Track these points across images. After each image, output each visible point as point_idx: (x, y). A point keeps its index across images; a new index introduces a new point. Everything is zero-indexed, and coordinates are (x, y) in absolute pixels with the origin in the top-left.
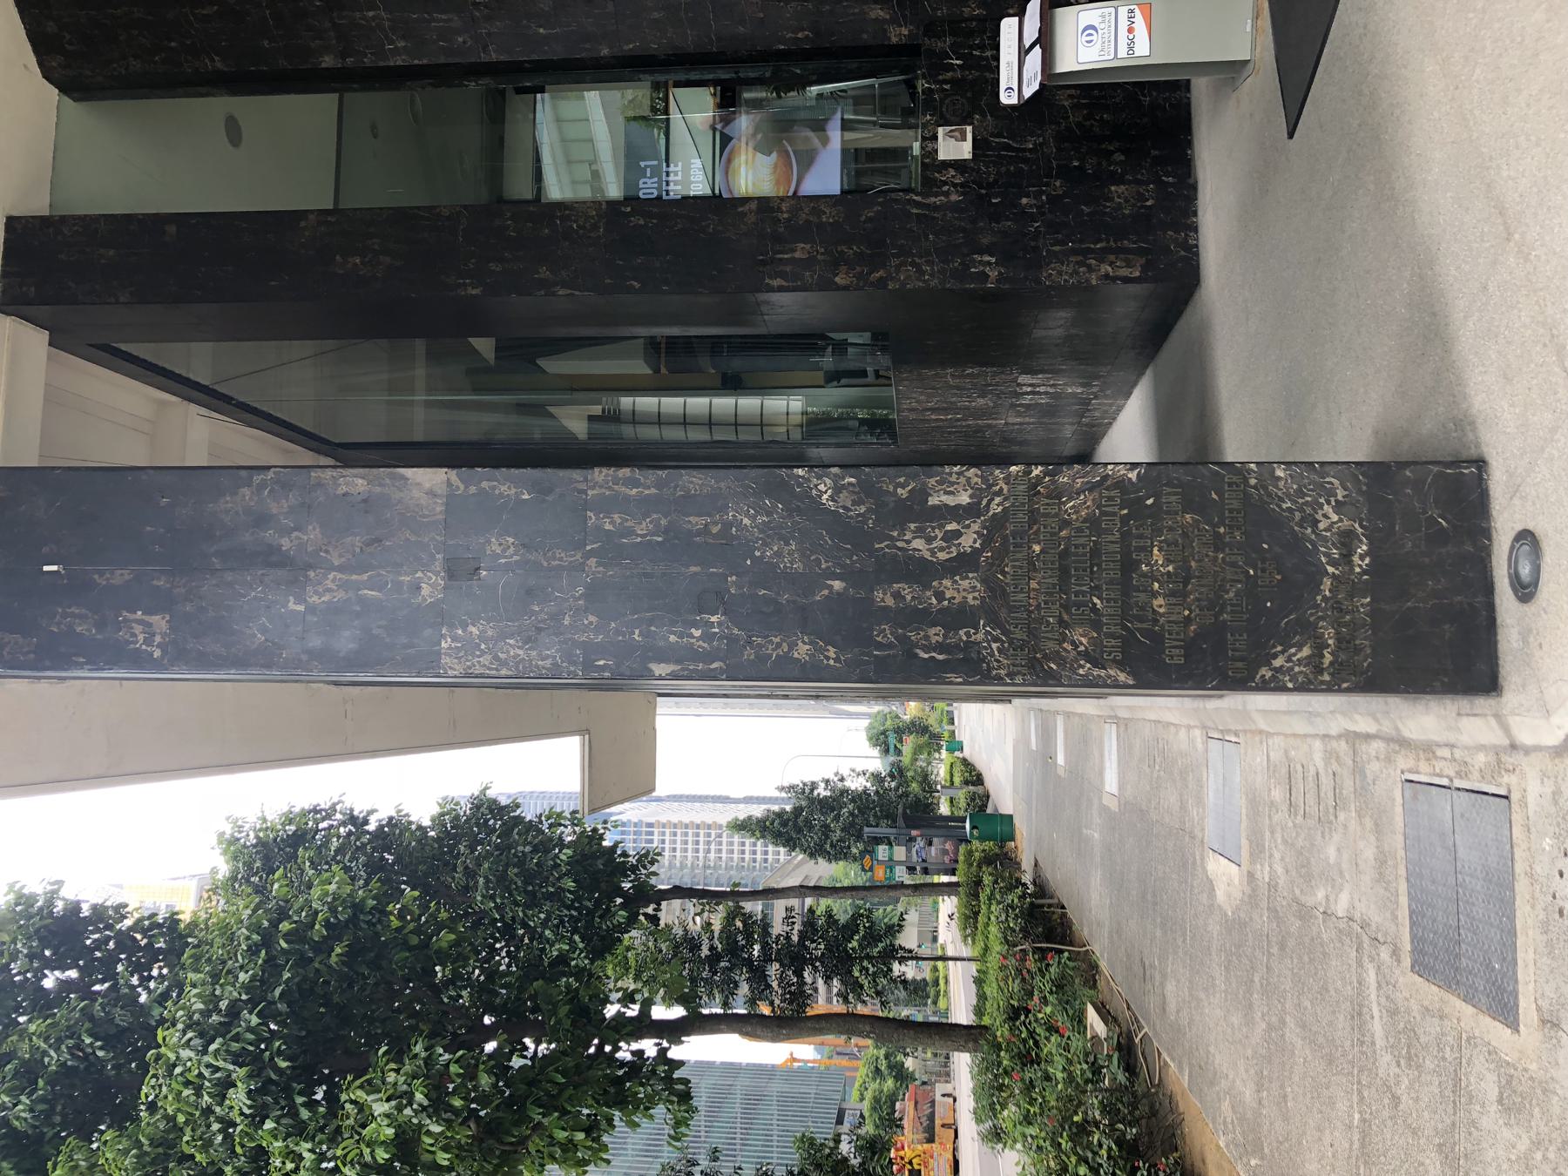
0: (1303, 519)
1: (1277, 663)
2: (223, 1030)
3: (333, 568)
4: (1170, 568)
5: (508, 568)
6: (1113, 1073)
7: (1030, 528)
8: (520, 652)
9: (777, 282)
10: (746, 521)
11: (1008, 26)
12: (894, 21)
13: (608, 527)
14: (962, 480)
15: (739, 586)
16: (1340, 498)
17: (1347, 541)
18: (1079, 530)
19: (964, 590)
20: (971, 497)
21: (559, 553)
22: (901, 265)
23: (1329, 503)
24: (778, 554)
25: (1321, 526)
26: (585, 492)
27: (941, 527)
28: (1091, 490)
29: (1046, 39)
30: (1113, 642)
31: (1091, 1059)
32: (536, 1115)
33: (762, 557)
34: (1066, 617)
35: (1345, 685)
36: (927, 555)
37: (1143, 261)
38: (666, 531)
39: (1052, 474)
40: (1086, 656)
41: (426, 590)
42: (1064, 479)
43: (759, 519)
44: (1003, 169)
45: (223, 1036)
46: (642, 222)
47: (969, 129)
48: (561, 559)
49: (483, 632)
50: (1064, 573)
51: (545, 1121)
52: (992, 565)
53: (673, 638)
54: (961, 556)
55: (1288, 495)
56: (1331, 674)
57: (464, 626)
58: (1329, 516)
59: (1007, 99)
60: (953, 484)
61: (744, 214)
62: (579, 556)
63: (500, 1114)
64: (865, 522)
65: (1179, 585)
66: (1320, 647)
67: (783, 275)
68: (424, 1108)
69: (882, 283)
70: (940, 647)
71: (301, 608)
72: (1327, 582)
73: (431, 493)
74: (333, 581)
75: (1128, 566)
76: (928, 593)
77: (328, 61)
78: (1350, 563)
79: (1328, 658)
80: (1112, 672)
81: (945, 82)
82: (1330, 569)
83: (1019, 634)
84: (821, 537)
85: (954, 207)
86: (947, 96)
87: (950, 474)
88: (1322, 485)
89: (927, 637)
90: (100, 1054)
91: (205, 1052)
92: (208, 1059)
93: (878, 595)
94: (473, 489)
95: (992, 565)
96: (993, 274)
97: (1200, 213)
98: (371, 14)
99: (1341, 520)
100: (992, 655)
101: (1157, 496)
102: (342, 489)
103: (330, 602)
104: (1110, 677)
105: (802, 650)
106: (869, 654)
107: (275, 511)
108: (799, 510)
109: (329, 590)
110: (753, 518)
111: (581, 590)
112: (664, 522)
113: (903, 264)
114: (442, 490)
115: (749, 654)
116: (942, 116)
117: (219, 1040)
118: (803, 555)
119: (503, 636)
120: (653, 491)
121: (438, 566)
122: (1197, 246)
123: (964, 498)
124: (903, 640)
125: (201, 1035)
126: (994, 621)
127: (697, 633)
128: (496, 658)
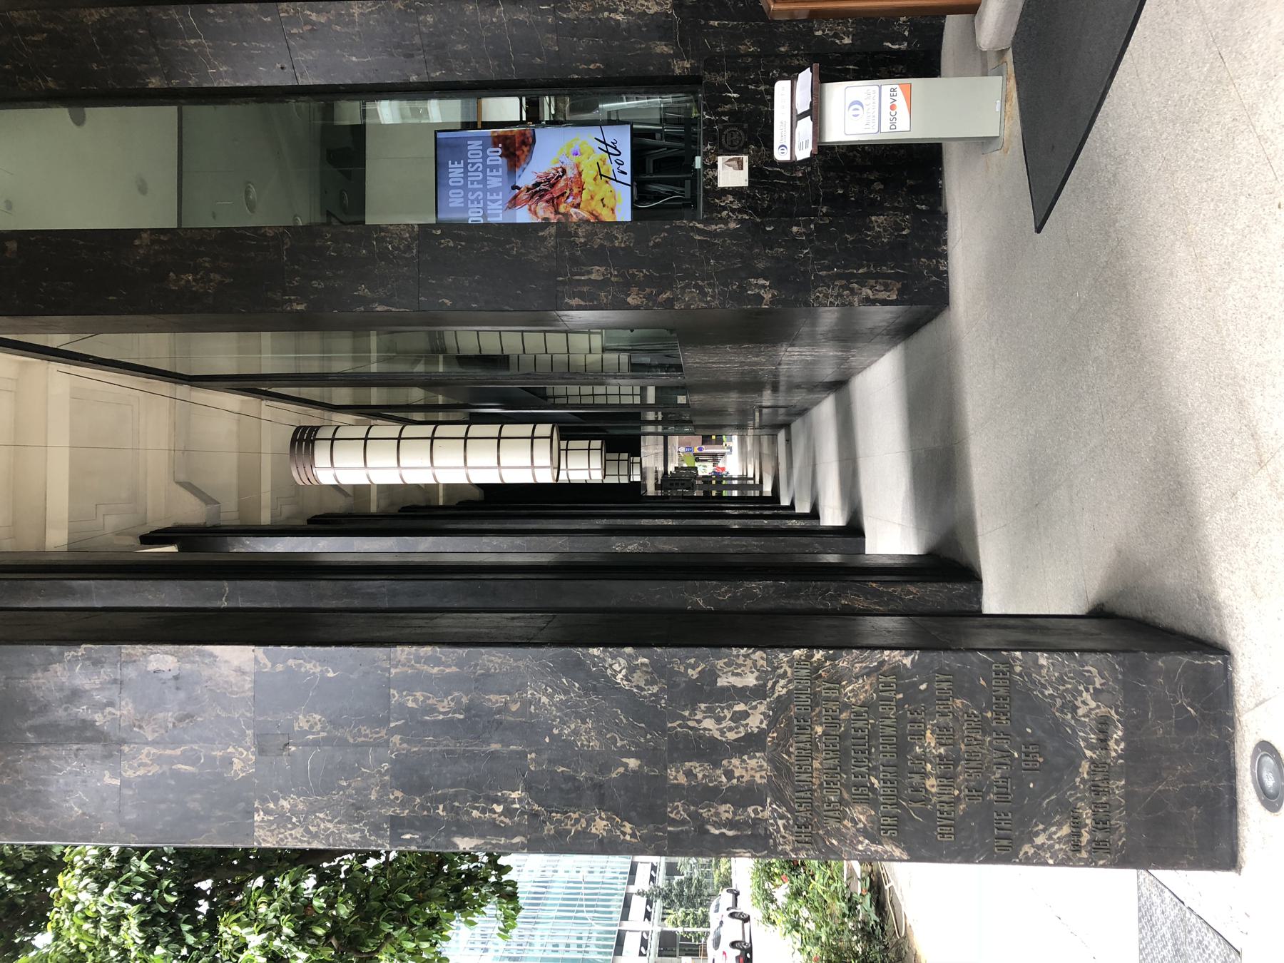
0: (1063, 706)
1: (1039, 840)
2: (115, 875)
3: (147, 743)
4: (942, 750)
5: (316, 743)
6: (866, 907)
7: (813, 710)
8: (330, 825)
9: (574, 302)
10: (544, 700)
11: (782, 89)
12: (677, 56)
13: (410, 704)
14: (749, 662)
15: (538, 764)
16: (1098, 686)
17: (1103, 726)
18: (858, 714)
19: (752, 769)
20: (757, 679)
21: (365, 730)
22: (683, 288)
23: (1087, 690)
24: (576, 732)
25: (1080, 712)
26: (388, 670)
27: (730, 707)
28: (868, 675)
29: (816, 112)
30: (890, 821)
31: (848, 896)
32: (387, 928)
33: (560, 735)
34: (846, 796)
35: (1101, 862)
36: (717, 735)
37: (899, 285)
38: (468, 709)
39: (833, 659)
40: (865, 833)
41: (238, 764)
42: (843, 664)
43: (557, 698)
44: (776, 196)
45: (116, 879)
46: (451, 244)
47: (746, 158)
48: (366, 736)
49: (294, 806)
50: (843, 755)
51: (396, 934)
52: (778, 745)
53: (475, 813)
54: (749, 737)
55: (1050, 683)
56: (1089, 852)
57: (276, 800)
58: (1088, 704)
59: (781, 155)
60: (740, 666)
61: (544, 239)
62: (383, 733)
63: (358, 928)
64: (657, 701)
65: (948, 765)
66: (1077, 826)
67: (581, 295)
68: (291, 939)
69: (669, 303)
70: (730, 824)
71: (117, 782)
72: (1085, 767)
73: (240, 671)
74: (148, 755)
75: (902, 748)
76: (718, 772)
77: (154, 82)
78: (1106, 748)
79: (1086, 837)
80: (888, 848)
81: (724, 114)
82: (1088, 753)
83: (803, 815)
84: (617, 716)
85: (732, 234)
86: (725, 128)
87: (737, 656)
88: (1081, 674)
89: (717, 814)
90: (11, 886)
91: (100, 892)
92: (101, 899)
93: (671, 773)
94: (280, 667)
95: (778, 745)
96: (767, 296)
97: (950, 243)
98: (193, 41)
99: (1098, 707)
100: (778, 831)
101: (930, 682)
102: (152, 667)
103: (145, 776)
104: (886, 852)
105: (600, 826)
106: (664, 831)
107: (87, 687)
108: (595, 689)
109: (145, 765)
110: (551, 697)
111: (386, 766)
112: (465, 700)
113: (688, 286)
114: (250, 667)
115: (549, 829)
116: (721, 146)
117: (112, 884)
118: (600, 733)
119: (312, 810)
120: (454, 669)
121: (249, 740)
122: (946, 272)
123: (751, 680)
124: (695, 816)
125: (96, 880)
126: (780, 799)
127: (499, 809)
128: (307, 831)
